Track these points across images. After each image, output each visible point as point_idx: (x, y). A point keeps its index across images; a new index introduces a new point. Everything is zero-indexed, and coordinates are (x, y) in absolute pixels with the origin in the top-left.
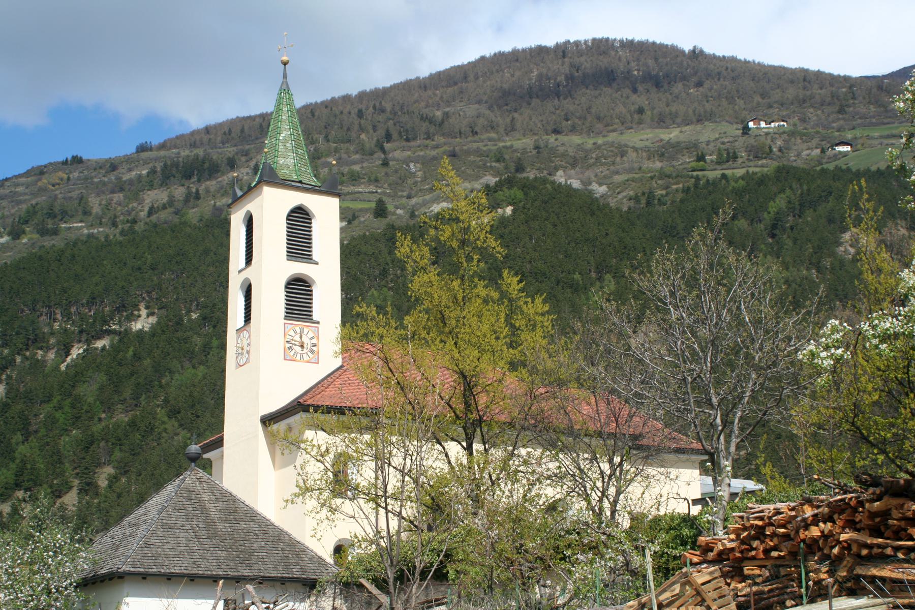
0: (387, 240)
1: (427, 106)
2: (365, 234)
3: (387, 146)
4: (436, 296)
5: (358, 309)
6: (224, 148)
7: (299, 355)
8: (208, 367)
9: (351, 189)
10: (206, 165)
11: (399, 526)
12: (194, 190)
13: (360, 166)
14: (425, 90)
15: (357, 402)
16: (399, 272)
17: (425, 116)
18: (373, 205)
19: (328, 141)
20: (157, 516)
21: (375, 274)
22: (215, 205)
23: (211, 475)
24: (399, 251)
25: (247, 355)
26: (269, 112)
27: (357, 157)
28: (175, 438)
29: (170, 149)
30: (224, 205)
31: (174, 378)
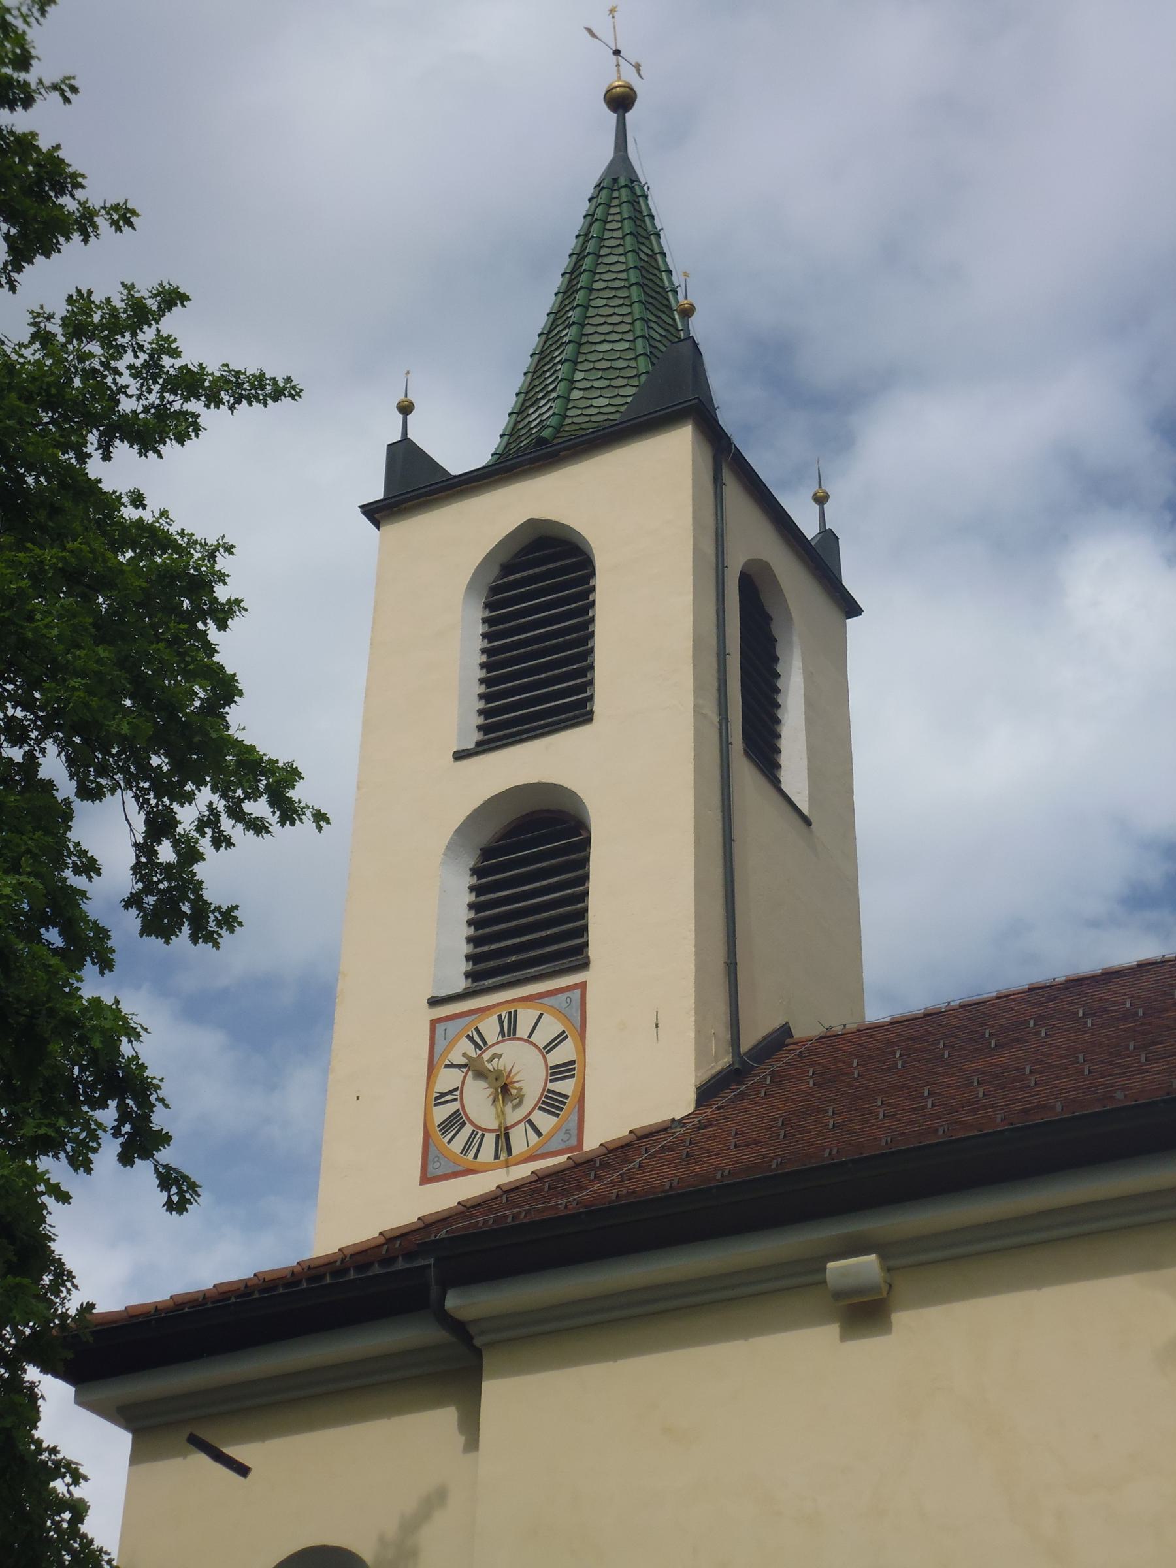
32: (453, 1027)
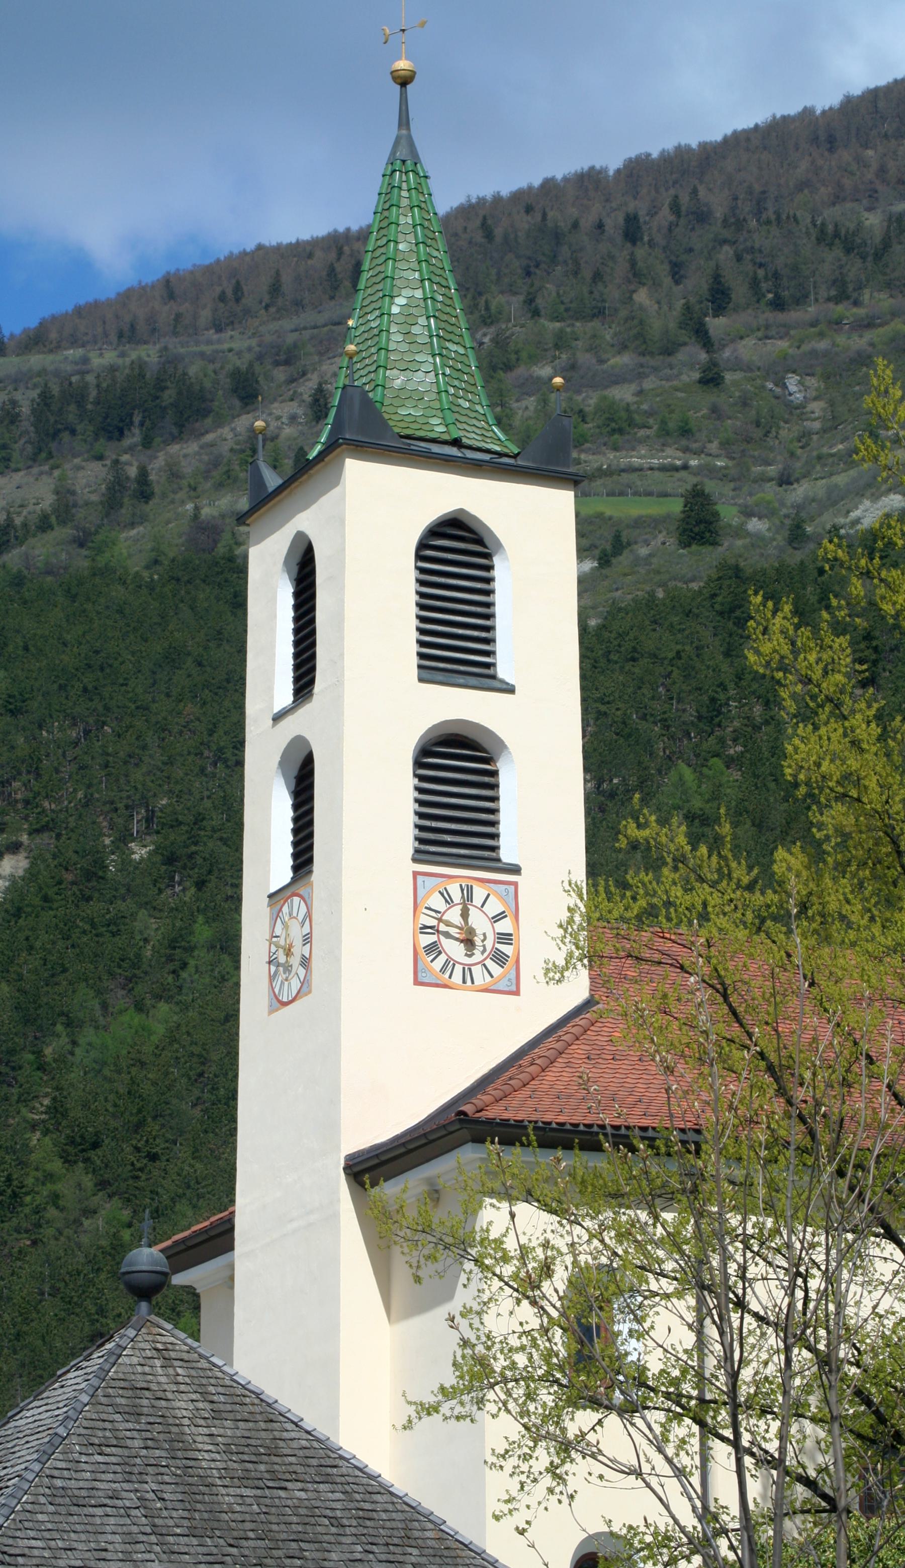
0: (721, 614)
1: (837, 199)
2: (652, 594)
3: (716, 325)
4: (872, 783)
5: (632, 830)
6: (219, 341)
7: (458, 969)
8: (185, 1007)
9: (608, 458)
10: (169, 396)
11: (778, 1501)
12: (133, 472)
13: (634, 387)
14: (831, 150)
15: (638, 1111)
16: (758, 710)
17: (830, 228)
18: (676, 507)
19: (536, 313)
20: (37, 1467)
21: (686, 718)
22: (196, 516)
23: (198, 1340)
24: (757, 652)
25: (302, 972)
26: (355, 228)
27: (624, 360)
28: (86, 1223)
29: (58, 347)
30: (223, 516)
31: (82, 1041)
32: (431, 882)
